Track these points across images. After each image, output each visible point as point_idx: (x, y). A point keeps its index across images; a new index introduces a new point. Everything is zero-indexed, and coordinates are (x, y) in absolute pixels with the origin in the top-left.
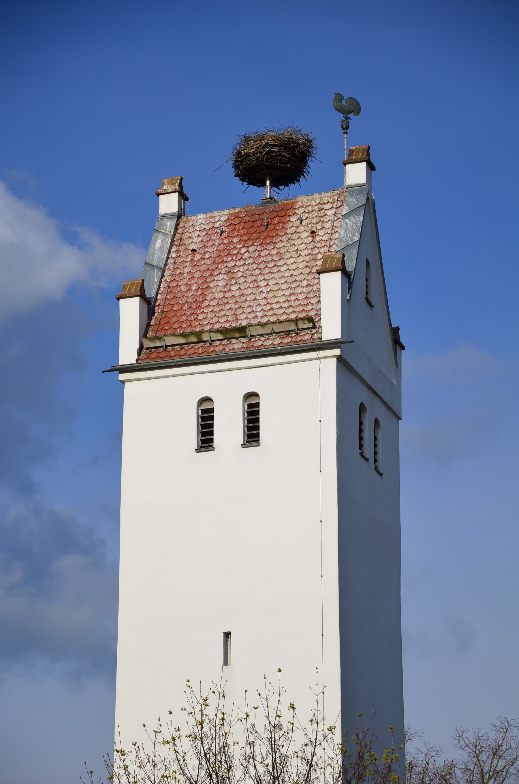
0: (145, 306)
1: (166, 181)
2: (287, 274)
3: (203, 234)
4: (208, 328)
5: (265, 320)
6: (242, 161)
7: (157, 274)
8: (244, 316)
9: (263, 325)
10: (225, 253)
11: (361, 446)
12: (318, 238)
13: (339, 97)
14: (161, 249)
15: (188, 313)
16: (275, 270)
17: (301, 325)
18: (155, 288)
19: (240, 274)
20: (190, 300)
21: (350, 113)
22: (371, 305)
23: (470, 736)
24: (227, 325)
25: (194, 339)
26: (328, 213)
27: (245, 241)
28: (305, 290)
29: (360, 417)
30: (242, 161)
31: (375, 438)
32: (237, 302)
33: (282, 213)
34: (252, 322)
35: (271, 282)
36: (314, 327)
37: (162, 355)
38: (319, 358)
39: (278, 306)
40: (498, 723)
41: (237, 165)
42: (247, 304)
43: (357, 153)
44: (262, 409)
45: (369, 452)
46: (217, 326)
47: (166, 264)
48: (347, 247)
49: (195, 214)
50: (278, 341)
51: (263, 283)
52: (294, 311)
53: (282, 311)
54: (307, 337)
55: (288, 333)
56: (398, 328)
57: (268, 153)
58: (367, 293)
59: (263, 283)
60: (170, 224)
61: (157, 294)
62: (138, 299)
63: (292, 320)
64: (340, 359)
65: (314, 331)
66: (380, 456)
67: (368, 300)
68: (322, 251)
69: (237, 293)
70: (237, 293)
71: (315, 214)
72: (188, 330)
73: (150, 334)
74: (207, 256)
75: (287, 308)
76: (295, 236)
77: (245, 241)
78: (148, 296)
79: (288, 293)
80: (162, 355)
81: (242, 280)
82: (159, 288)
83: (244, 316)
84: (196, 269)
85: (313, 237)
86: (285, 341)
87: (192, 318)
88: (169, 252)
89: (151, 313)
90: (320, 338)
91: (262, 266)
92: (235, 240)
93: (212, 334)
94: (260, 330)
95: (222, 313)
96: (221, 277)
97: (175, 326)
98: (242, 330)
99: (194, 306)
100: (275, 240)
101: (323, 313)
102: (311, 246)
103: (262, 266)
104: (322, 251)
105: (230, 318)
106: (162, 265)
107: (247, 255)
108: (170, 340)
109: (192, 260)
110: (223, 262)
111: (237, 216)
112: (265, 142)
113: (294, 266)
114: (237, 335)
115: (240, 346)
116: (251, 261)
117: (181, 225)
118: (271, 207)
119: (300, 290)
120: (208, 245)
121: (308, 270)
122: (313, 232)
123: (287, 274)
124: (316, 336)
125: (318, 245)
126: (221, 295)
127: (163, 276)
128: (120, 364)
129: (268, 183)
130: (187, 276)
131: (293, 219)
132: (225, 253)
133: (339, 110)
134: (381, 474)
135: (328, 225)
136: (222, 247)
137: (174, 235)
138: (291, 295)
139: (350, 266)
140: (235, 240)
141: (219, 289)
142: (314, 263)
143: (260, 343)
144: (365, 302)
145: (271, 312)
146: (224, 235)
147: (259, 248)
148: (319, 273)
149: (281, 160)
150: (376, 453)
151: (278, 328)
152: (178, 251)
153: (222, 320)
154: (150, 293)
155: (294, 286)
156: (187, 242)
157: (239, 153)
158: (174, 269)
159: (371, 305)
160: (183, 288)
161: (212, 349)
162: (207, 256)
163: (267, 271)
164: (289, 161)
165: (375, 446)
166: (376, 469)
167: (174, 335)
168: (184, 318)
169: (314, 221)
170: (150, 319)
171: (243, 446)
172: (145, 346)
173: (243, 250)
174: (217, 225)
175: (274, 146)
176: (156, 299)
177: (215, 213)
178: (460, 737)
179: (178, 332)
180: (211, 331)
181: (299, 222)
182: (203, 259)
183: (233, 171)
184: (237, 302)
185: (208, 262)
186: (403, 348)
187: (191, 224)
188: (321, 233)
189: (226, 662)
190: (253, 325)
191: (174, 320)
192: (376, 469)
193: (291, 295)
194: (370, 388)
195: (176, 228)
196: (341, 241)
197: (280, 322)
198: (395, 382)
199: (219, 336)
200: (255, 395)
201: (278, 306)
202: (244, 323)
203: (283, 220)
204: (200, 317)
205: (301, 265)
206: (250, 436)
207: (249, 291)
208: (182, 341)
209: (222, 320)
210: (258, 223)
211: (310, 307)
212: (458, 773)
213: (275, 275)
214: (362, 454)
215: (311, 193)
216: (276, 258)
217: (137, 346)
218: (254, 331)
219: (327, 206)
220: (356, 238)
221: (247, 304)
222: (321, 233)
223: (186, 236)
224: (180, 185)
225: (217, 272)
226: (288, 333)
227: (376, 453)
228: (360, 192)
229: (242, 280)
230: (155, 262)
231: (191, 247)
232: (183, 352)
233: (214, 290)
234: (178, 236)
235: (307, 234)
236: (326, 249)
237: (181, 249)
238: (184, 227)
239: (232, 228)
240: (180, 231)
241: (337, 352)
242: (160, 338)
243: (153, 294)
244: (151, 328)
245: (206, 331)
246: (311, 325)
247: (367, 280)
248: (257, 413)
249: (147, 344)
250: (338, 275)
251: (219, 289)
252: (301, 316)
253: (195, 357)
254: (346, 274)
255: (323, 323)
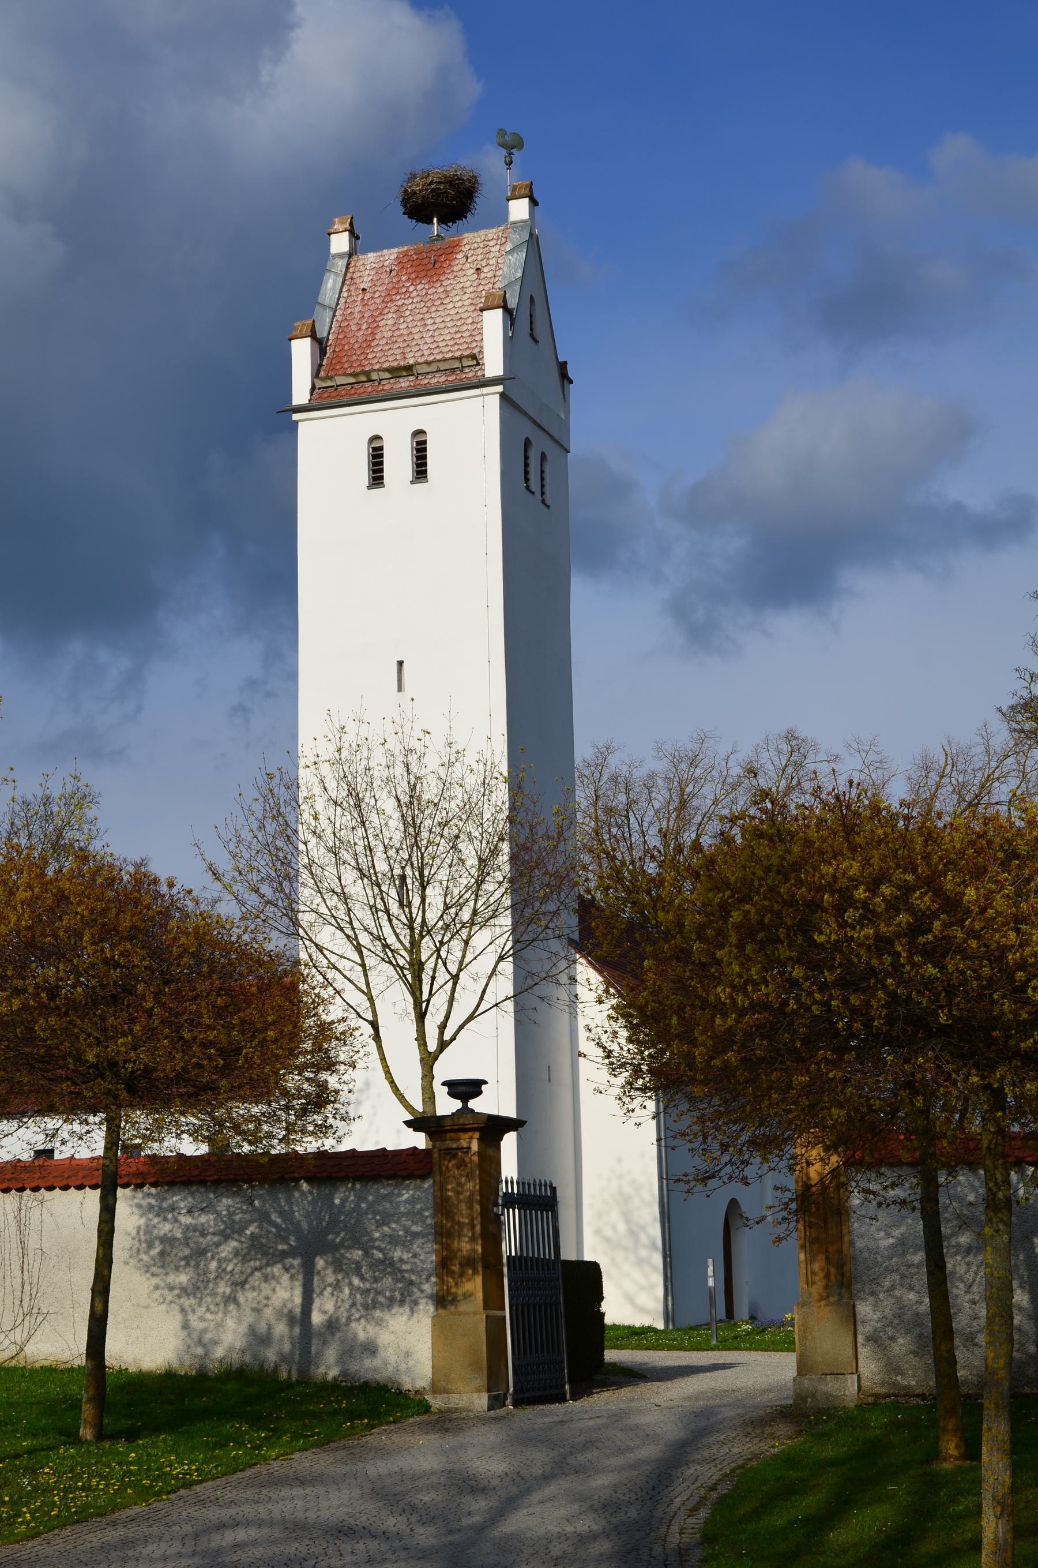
0: (317, 346)
1: (337, 220)
2: (453, 312)
3: (373, 273)
4: (377, 367)
5: (431, 358)
6: (409, 199)
7: (329, 314)
8: (412, 354)
9: (428, 363)
10: (394, 292)
11: (527, 480)
12: (483, 275)
13: (502, 132)
14: (333, 288)
15: (359, 353)
16: (441, 308)
17: (466, 362)
18: (327, 328)
19: (408, 313)
20: (360, 340)
21: (513, 148)
22: (536, 341)
23: (668, 748)
24: (395, 364)
25: (364, 379)
26: (493, 249)
27: (413, 280)
28: (469, 328)
29: (526, 451)
30: (409, 199)
31: (542, 472)
32: (405, 341)
33: (449, 251)
34: (420, 360)
35: (438, 320)
36: (478, 364)
37: (333, 394)
38: (482, 395)
39: (444, 344)
40: (695, 735)
41: (404, 203)
42: (415, 342)
43: (521, 188)
44: (429, 446)
45: (535, 484)
46: (386, 365)
47: (338, 304)
48: (510, 284)
49: (365, 252)
50: (443, 379)
51: (430, 322)
52: (459, 349)
53: (447, 349)
54: (471, 375)
55: (453, 370)
56: (566, 363)
57: (433, 190)
58: (532, 329)
59: (430, 322)
60: (341, 264)
61: (329, 334)
62: (309, 339)
63: (456, 358)
64: (503, 396)
65: (477, 368)
66: (547, 490)
67: (532, 336)
68: (486, 288)
69: (405, 332)
70: (405, 332)
71: (480, 251)
72: (358, 370)
73: (322, 374)
74: (377, 295)
75: (452, 346)
76: (461, 274)
77: (413, 280)
78: (319, 336)
79: (453, 330)
80: (333, 394)
81: (410, 318)
82: (331, 328)
83: (412, 354)
84: (366, 308)
85: (478, 274)
86: (450, 379)
87: (362, 357)
88: (341, 291)
89: (323, 352)
90: (484, 375)
91: (429, 304)
92: (404, 278)
93: (381, 373)
94: (425, 369)
95: (391, 352)
96: (390, 315)
97: (346, 365)
98: (409, 369)
99: (364, 345)
100: (443, 278)
101: (485, 350)
102: (476, 283)
103: (429, 304)
104: (486, 288)
105: (398, 357)
106: (333, 305)
107: (415, 293)
108: (341, 380)
109: (363, 299)
110: (392, 300)
111: (406, 254)
112: (430, 179)
113: (459, 304)
114: (405, 374)
115: (408, 384)
116: (419, 299)
117: (352, 264)
118: (438, 245)
119: (465, 327)
120: (378, 284)
121: (473, 308)
122: (478, 269)
123: (453, 312)
124: (479, 373)
125: (483, 282)
126: (390, 334)
127: (334, 316)
128: (294, 403)
129: (435, 220)
130: (357, 316)
131: (459, 256)
132: (394, 292)
133: (503, 145)
134: (548, 507)
135: (493, 262)
136: (391, 285)
137: (345, 274)
138: (456, 332)
139: (512, 303)
140: (404, 278)
141: (388, 328)
142: (478, 300)
143: (426, 381)
144: (529, 337)
145: (437, 350)
146: (393, 274)
147: (427, 286)
148: (482, 310)
149: (447, 197)
150: (542, 486)
151: (443, 366)
152: (349, 291)
153: (391, 358)
154: (322, 333)
155: (459, 323)
156: (358, 281)
157: (406, 191)
158: (345, 309)
159: (536, 341)
160: (354, 328)
161: (381, 388)
162: (377, 295)
163: (433, 309)
164: (454, 198)
165: (542, 479)
166: (543, 501)
167: (345, 374)
168: (355, 358)
169: (479, 258)
170: (322, 359)
171: (412, 482)
172: (317, 386)
173: (412, 288)
174: (386, 264)
175: (439, 183)
176: (328, 339)
177: (385, 251)
178: (659, 749)
179: (349, 371)
180: (379, 370)
181: (464, 259)
182: (373, 298)
183: (401, 209)
184: (405, 341)
185: (378, 301)
186: (571, 382)
187: (361, 262)
188: (485, 270)
189: (400, 689)
190: (420, 364)
191: (345, 359)
192: (543, 501)
193: (456, 332)
194: (535, 423)
195: (347, 268)
196: (504, 278)
197: (445, 360)
198: (563, 416)
199: (388, 375)
200: (422, 432)
201: (444, 344)
202: (411, 362)
203: (450, 257)
204: (370, 356)
205: (466, 303)
206: (419, 473)
207: (417, 330)
208: (352, 380)
209: (391, 358)
210: (426, 261)
211: (474, 344)
212: (660, 782)
213: (442, 313)
214: (528, 488)
215: (476, 229)
216: (441, 296)
217: (309, 386)
218: (421, 369)
219: (492, 243)
220: (519, 274)
221: (415, 342)
222: (485, 270)
223: (356, 275)
224: (351, 224)
225: (386, 311)
226: (453, 370)
227: (542, 486)
228: (523, 228)
229: (410, 318)
230: (327, 302)
231: (362, 286)
232: (353, 391)
233: (383, 329)
234: (349, 275)
235: (472, 271)
236: (490, 286)
237: (352, 288)
238: (355, 266)
239: (401, 266)
240: (351, 270)
241: (500, 388)
242: (331, 378)
243: (325, 335)
244: (323, 368)
245: (375, 370)
246: (475, 362)
247: (531, 316)
248: (425, 449)
249: (319, 384)
250: (500, 312)
251: (388, 328)
252: (466, 353)
253: (365, 396)
254: (507, 311)
255: (486, 360)
